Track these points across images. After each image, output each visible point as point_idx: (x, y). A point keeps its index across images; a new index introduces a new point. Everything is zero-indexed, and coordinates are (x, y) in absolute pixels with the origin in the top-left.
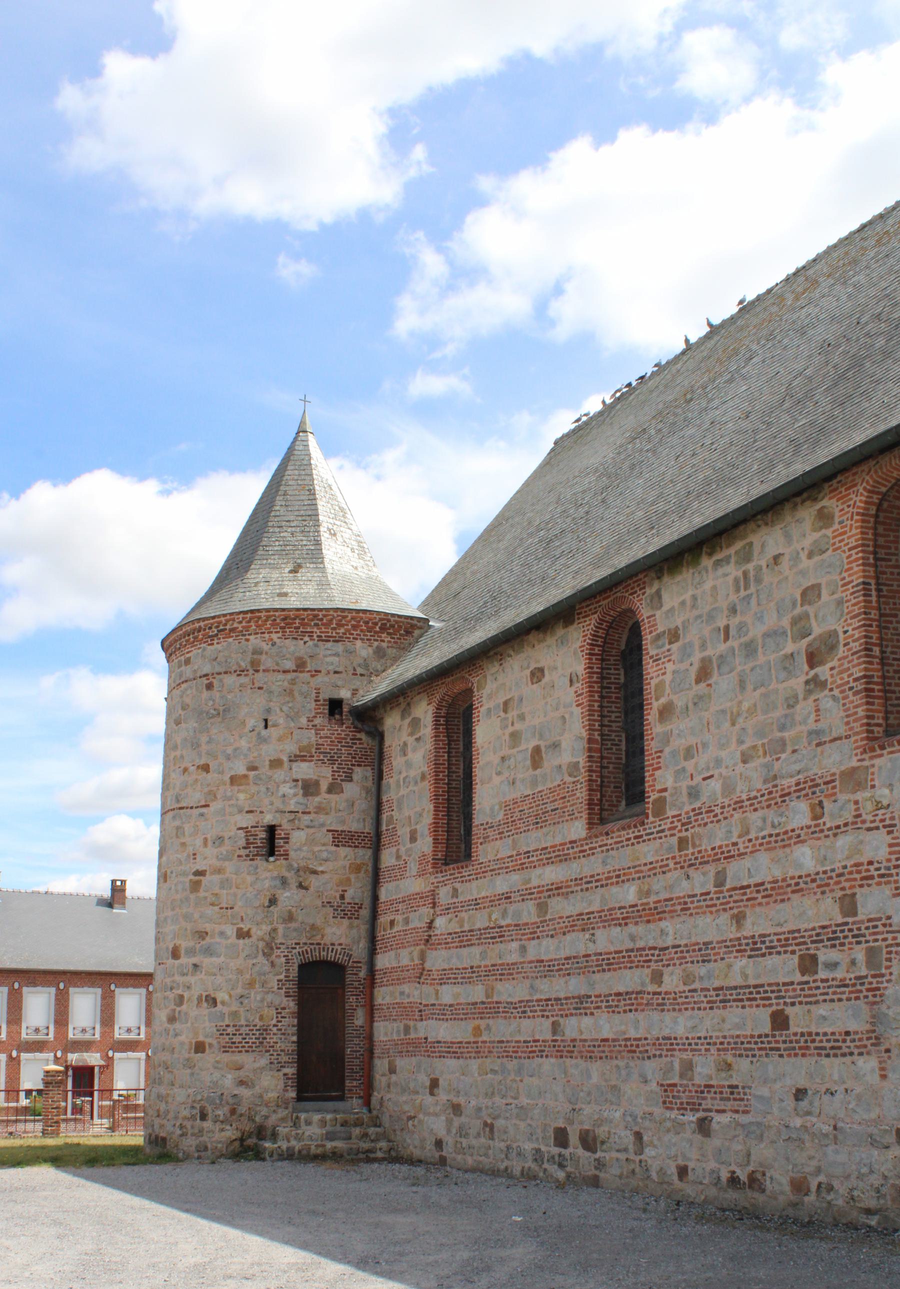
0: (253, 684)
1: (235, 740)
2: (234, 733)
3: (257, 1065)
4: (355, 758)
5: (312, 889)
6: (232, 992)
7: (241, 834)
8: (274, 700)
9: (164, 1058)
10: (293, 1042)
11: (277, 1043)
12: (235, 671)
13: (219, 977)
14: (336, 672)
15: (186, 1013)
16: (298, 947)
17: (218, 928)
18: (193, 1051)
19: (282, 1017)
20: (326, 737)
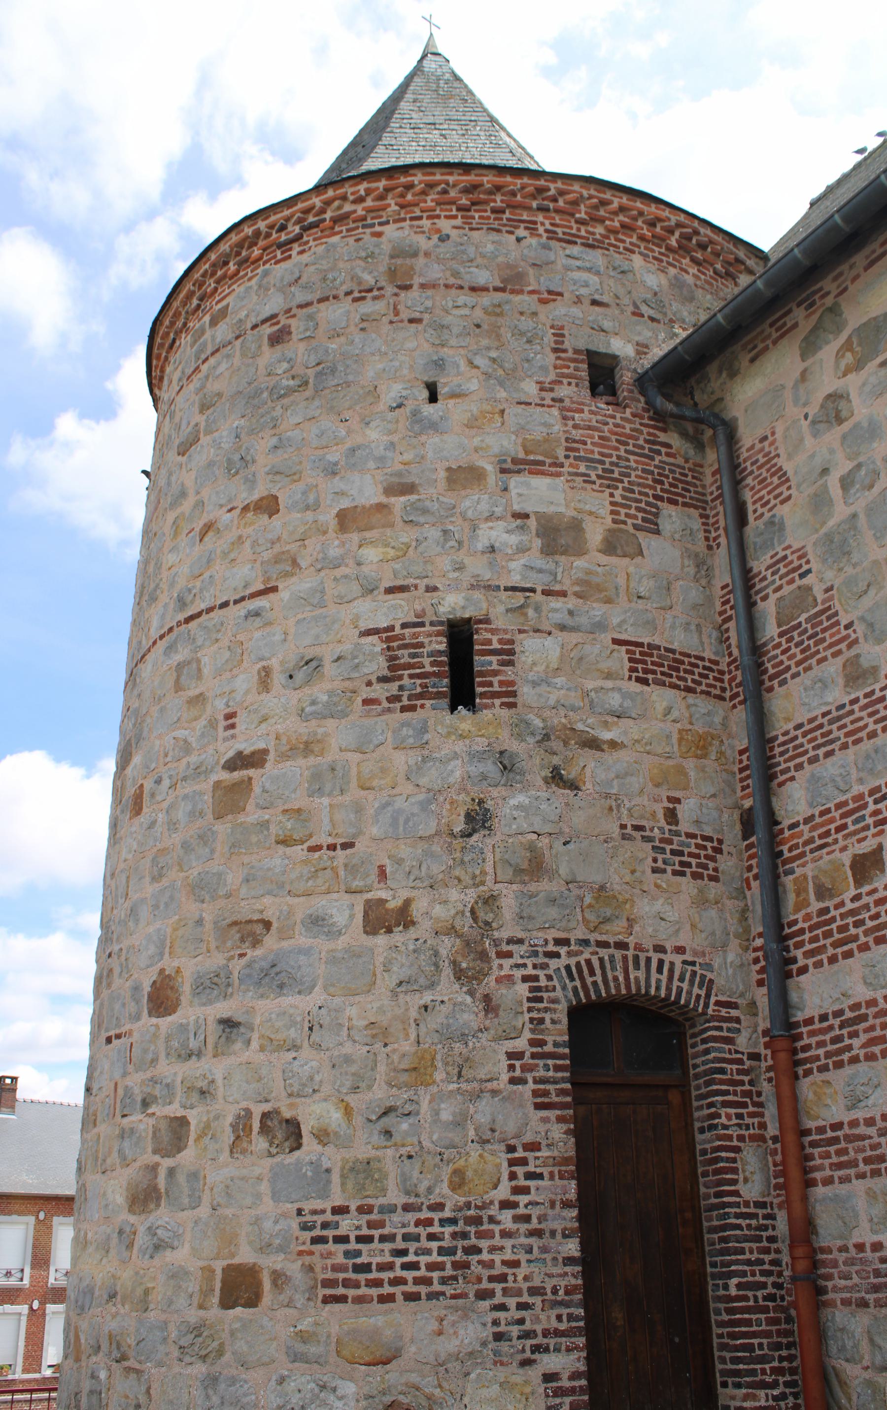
0: (397, 314)
1: (349, 432)
2: (347, 415)
3: (449, 1345)
4: (661, 483)
5: (588, 786)
6: (352, 1100)
7: (375, 644)
8: (453, 342)
9: (113, 1325)
10: (569, 1261)
11: (516, 1264)
12: (348, 294)
13: (306, 1052)
14: (594, 303)
15: (194, 1176)
16: (563, 950)
17: (302, 907)
18: (215, 1300)
19: (530, 1176)
20: (589, 428)
